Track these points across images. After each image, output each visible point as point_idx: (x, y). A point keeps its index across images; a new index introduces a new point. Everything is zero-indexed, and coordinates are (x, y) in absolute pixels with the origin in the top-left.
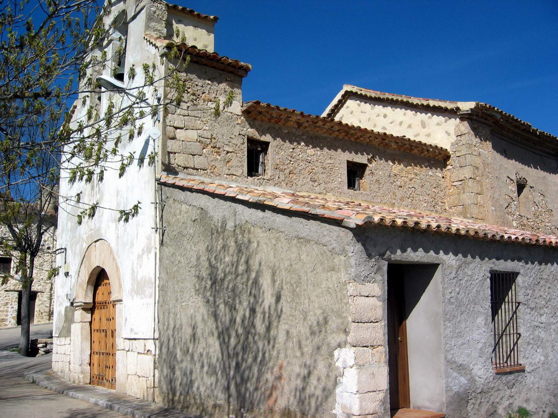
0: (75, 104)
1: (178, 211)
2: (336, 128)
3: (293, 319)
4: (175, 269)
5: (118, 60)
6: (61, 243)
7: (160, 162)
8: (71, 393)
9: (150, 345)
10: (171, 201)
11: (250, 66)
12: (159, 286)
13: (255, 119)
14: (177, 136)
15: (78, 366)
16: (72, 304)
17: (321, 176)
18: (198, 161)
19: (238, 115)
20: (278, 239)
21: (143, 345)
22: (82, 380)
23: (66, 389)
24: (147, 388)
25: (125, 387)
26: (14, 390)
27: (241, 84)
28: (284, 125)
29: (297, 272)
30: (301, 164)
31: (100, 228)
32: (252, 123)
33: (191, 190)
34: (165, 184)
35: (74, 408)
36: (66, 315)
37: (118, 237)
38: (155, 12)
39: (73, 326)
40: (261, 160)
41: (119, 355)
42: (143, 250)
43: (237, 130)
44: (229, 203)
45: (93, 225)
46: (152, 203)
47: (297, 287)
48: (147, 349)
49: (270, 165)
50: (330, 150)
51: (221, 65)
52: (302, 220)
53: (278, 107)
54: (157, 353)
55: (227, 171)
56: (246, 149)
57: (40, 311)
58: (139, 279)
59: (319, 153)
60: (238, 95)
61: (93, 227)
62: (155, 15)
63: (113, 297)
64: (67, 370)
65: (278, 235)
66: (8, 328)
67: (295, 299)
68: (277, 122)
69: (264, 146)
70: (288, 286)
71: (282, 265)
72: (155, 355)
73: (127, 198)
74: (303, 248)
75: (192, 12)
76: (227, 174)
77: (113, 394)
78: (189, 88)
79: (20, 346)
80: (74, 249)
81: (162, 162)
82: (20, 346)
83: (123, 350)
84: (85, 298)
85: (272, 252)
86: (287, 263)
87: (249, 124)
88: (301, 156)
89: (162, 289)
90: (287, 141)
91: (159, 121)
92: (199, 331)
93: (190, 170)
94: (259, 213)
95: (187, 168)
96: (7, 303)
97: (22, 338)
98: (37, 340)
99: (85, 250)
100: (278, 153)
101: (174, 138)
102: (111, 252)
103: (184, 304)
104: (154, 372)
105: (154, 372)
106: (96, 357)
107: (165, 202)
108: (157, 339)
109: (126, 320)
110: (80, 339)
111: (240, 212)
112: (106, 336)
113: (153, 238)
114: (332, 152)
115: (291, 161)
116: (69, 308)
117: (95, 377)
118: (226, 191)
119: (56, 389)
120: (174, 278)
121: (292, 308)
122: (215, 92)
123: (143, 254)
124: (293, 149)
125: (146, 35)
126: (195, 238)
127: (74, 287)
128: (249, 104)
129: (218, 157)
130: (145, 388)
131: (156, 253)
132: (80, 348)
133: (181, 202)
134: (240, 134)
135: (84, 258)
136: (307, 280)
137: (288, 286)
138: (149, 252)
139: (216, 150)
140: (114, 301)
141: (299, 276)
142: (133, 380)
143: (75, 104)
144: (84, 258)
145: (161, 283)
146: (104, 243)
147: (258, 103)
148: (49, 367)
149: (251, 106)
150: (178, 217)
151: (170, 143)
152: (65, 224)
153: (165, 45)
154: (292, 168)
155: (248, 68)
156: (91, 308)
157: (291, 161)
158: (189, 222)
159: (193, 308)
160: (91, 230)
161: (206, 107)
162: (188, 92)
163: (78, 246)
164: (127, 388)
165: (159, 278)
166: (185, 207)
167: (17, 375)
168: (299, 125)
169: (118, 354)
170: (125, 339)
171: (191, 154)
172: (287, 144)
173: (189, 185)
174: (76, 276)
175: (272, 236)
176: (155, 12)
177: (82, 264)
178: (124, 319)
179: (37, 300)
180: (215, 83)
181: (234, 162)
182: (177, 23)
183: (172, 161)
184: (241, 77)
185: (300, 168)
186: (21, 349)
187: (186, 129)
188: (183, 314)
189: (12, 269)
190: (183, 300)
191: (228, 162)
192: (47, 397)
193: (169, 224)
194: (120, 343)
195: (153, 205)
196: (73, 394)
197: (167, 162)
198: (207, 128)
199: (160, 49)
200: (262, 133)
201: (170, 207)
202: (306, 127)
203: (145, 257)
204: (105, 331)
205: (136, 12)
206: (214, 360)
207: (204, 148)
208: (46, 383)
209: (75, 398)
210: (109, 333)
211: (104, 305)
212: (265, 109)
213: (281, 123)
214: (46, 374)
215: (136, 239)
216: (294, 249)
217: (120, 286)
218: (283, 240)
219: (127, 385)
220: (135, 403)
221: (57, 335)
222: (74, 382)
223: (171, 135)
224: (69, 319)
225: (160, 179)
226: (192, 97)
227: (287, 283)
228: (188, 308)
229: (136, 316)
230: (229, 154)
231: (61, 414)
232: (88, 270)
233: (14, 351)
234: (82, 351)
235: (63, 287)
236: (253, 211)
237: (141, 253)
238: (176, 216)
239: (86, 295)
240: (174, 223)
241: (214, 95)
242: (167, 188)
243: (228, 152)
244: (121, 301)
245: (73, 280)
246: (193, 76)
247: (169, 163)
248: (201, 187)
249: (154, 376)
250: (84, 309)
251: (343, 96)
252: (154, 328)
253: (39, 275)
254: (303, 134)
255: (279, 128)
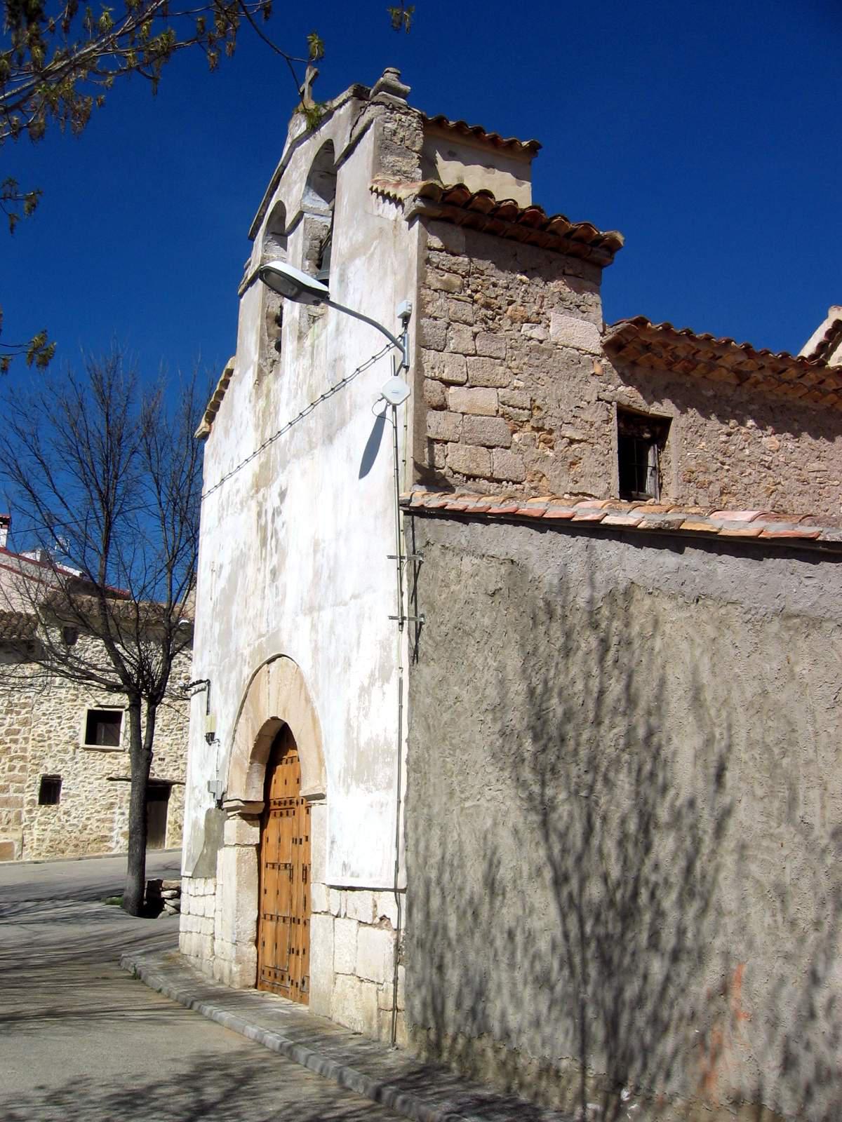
0: (229, 366)
1: (453, 575)
2: (831, 384)
3: (774, 845)
4: (446, 717)
5: (317, 255)
6: (200, 670)
7: (410, 462)
8: (208, 1009)
9: (388, 906)
10: (436, 551)
11: (620, 238)
12: (408, 762)
13: (634, 364)
14: (451, 402)
15: (230, 944)
16: (220, 803)
17: (797, 501)
18: (500, 462)
19: (594, 355)
20: (722, 624)
21: (371, 904)
22: (237, 979)
23: (204, 997)
24: (379, 1009)
25: (329, 1003)
26: (91, 994)
27: (598, 284)
28: (704, 377)
29: (784, 711)
30: (749, 471)
31: (279, 631)
32: (627, 373)
33: (483, 517)
34: (421, 512)
35: (210, 1048)
36: (208, 830)
37: (316, 650)
38: (395, 133)
39: (221, 853)
40: (651, 462)
41: (317, 924)
42: (372, 675)
43: (592, 390)
44: (582, 541)
45: (265, 625)
46: (391, 557)
47: (784, 754)
48: (380, 914)
49: (673, 472)
50: (817, 438)
51: (551, 236)
52: (796, 563)
53: (689, 333)
54: (403, 925)
55: (570, 487)
56: (615, 434)
57: (176, 822)
58: (362, 744)
59: (790, 445)
60: (594, 308)
61: (264, 631)
62: (395, 139)
63: (307, 789)
64: (207, 951)
65: (723, 611)
66: (114, 856)
67: (777, 788)
68: (687, 372)
69: (658, 430)
70: (756, 752)
71: (735, 694)
72: (398, 930)
73: (336, 556)
74: (800, 643)
75: (478, 132)
76: (571, 494)
77: (303, 1018)
78: (476, 291)
79: (126, 894)
80: (225, 682)
81: (415, 463)
82: (126, 894)
83: (326, 913)
84: (246, 792)
85: (706, 660)
86: (751, 689)
87: (622, 375)
88: (747, 452)
89: (416, 766)
90: (713, 417)
91: (407, 368)
92: (505, 874)
93: (482, 481)
94: (668, 559)
95: (475, 477)
96: (112, 803)
97: (130, 876)
98: (160, 882)
99: (247, 682)
100: (692, 445)
101: (442, 407)
102: (302, 685)
103: (467, 804)
104: (396, 973)
105: (396, 973)
106: (269, 926)
107: (421, 555)
108: (404, 891)
109: (333, 842)
110: (234, 883)
111: (614, 559)
112: (291, 878)
113: (395, 644)
114: (823, 444)
115: (723, 464)
116: (213, 812)
117: (267, 973)
118: (574, 510)
119: (178, 996)
120: (444, 739)
121: (769, 815)
122: (538, 301)
123: (372, 684)
124: (729, 435)
125: (376, 182)
126: (495, 636)
127: (224, 765)
128: (619, 327)
129: (550, 453)
130: (375, 1009)
131: (401, 682)
132: (235, 902)
133: (460, 552)
134: (599, 400)
135: (244, 701)
136: (816, 734)
137: (756, 752)
138: (386, 679)
139: (544, 435)
140: (309, 798)
141: (789, 723)
142: (346, 985)
143: (229, 366)
144: (244, 701)
145: (413, 752)
146: (287, 664)
147: (641, 322)
148: (173, 942)
149: (625, 330)
150: (453, 588)
151: (433, 418)
152: (208, 627)
153: (416, 191)
154: (726, 480)
155: (614, 241)
156: (259, 814)
157: (723, 464)
158: (482, 598)
159: (492, 807)
160: (261, 636)
161: (518, 334)
162: (475, 302)
163: (234, 675)
164: (334, 1006)
165: (407, 741)
166: (474, 559)
167: (102, 959)
168: (742, 377)
169: (315, 921)
170: (332, 887)
171: (484, 446)
172: (714, 423)
173: (479, 505)
174: (229, 741)
175: (704, 617)
176: (395, 133)
177: (240, 713)
178: (328, 841)
179: (170, 800)
180: (538, 280)
181: (588, 463)
182: (445, 159)
183: (439, 461)
184: (600, 265)
185: (746, 480)
186: (126, 899)
187: (472, 387)
188: (466, 830)
189: (121, 736)
190: (467, 794)
191: (573, 464)
192: (155, 1017)
193: (432, 607)
194: (320, 897)
195: (395, 563)
196: (211, 1012)
197: (426, 463)
198: (521, 384)
199: (406, 203)
200: (654, 395)
201: (435, 565)
202: (757, 383)
203: (376, 691)
204: (289, 867)
205: (353, 138)
206: (543, 945)
207: (514, 432)
208: (160, 980)
209: (216, 1022)
210: (298, 873)
211: (289, 807)
212: (659, 339)
213: (696, 374)
214: (164, 959)
215: (355, 649)
216: (772, 649)
217: (321, 762)
218: (737, 624)
219: (334, 999)
220: (351, 1044)
221: (190, 874)
222: (221, 981)
223: (437, 399)
224: (213, 839)
225: (410, 501)
226: (483, 311)
227: (751, 745)
228: (478, 815)
229: (357, 834)
230: (575, 446)
231: (172, 1066)
232: (253, 728)
233: (113, 903)
234: (239, 910)
235: (202, 766)
236: (648, 553)
237: (366, 684)
238: (447, 586)
239: (248, 784)
240: (444, 604)
241: (536, 308)
242: (426, 521)
243: (572, 442)
244: (322, 797)
245: (223, 750)
246: (485, 265)
247: (432, 466)
248: (509, 507)
249: (395, 982)
250: (244, 816)
251: (829, 334)
252: (397, 863)
253: (175, 748)
254: (751, 401)
255: (693, 385)
